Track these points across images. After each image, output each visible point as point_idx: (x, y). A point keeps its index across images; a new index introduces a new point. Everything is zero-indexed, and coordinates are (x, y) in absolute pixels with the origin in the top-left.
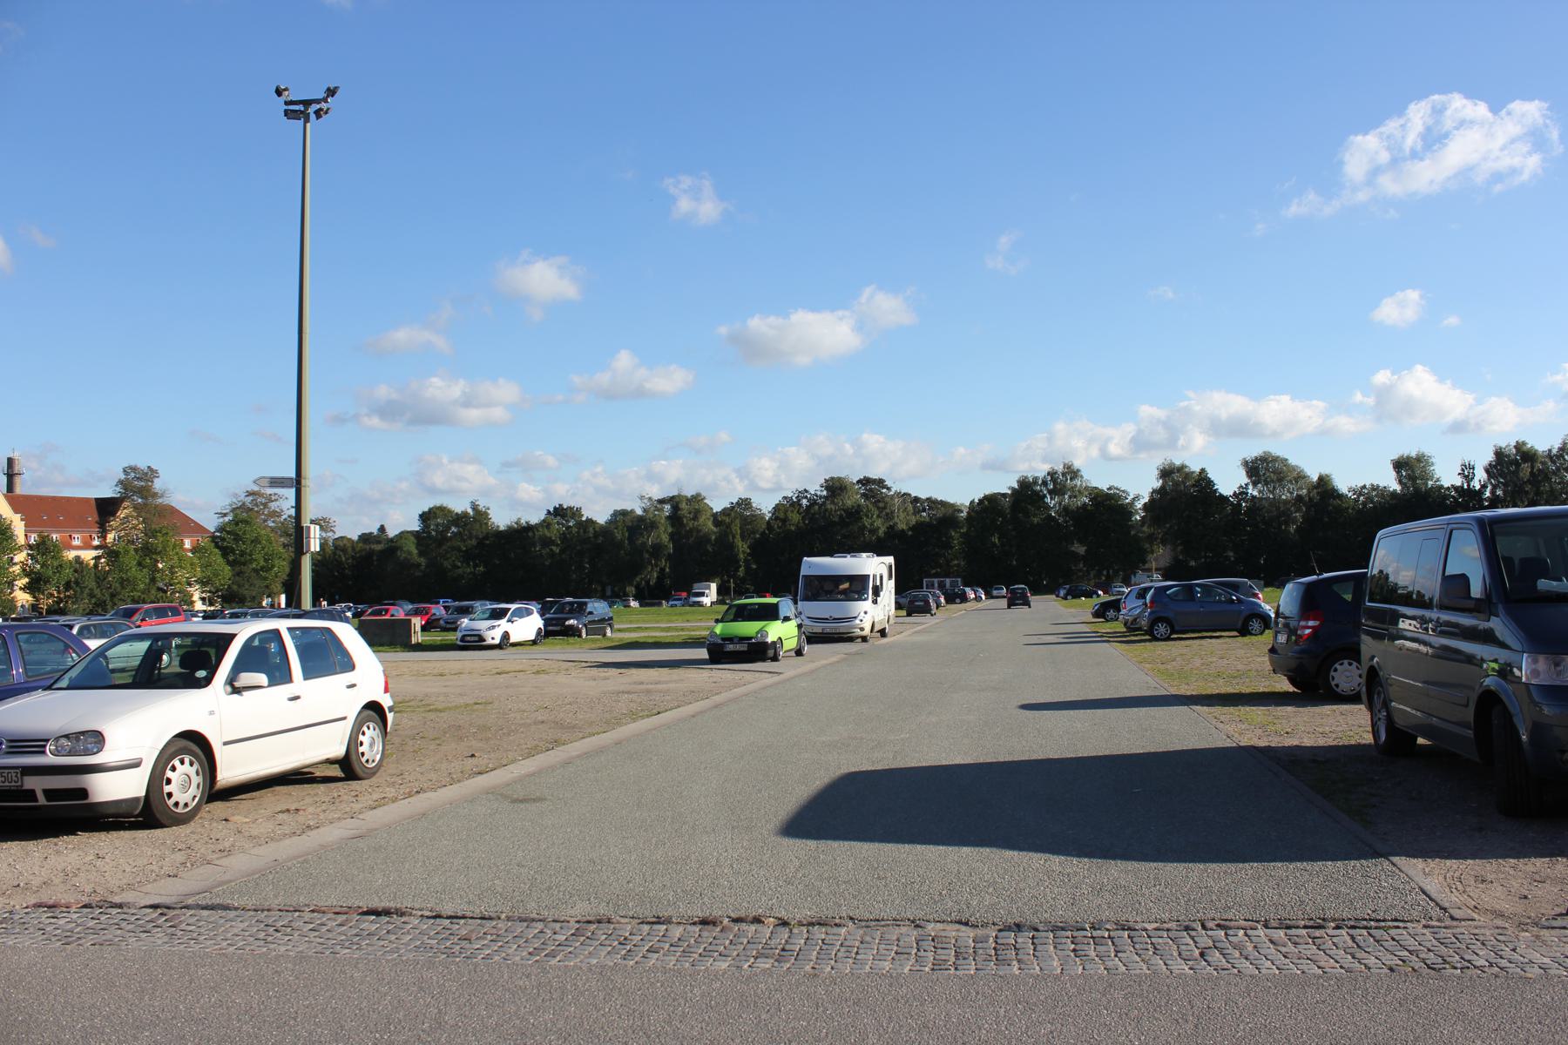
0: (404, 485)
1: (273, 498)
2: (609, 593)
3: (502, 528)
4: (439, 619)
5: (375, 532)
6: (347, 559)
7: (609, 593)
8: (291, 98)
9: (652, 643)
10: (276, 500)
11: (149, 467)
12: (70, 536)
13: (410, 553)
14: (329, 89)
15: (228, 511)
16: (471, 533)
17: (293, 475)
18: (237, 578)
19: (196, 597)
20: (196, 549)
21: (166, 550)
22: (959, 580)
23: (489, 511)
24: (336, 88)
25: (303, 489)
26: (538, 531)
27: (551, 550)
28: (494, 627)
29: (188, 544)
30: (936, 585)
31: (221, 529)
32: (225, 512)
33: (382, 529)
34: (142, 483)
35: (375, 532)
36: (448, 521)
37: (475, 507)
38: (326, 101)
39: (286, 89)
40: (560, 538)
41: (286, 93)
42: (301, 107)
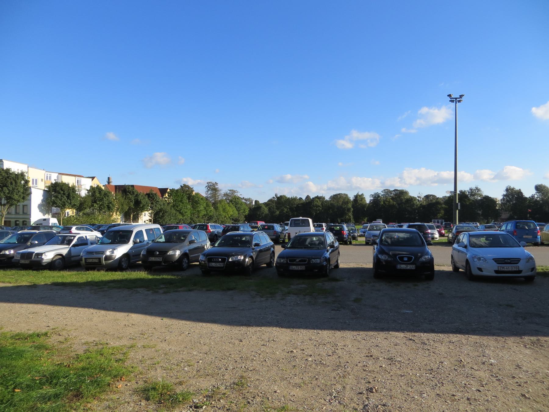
22: (443, 220)
30: (436, 222)
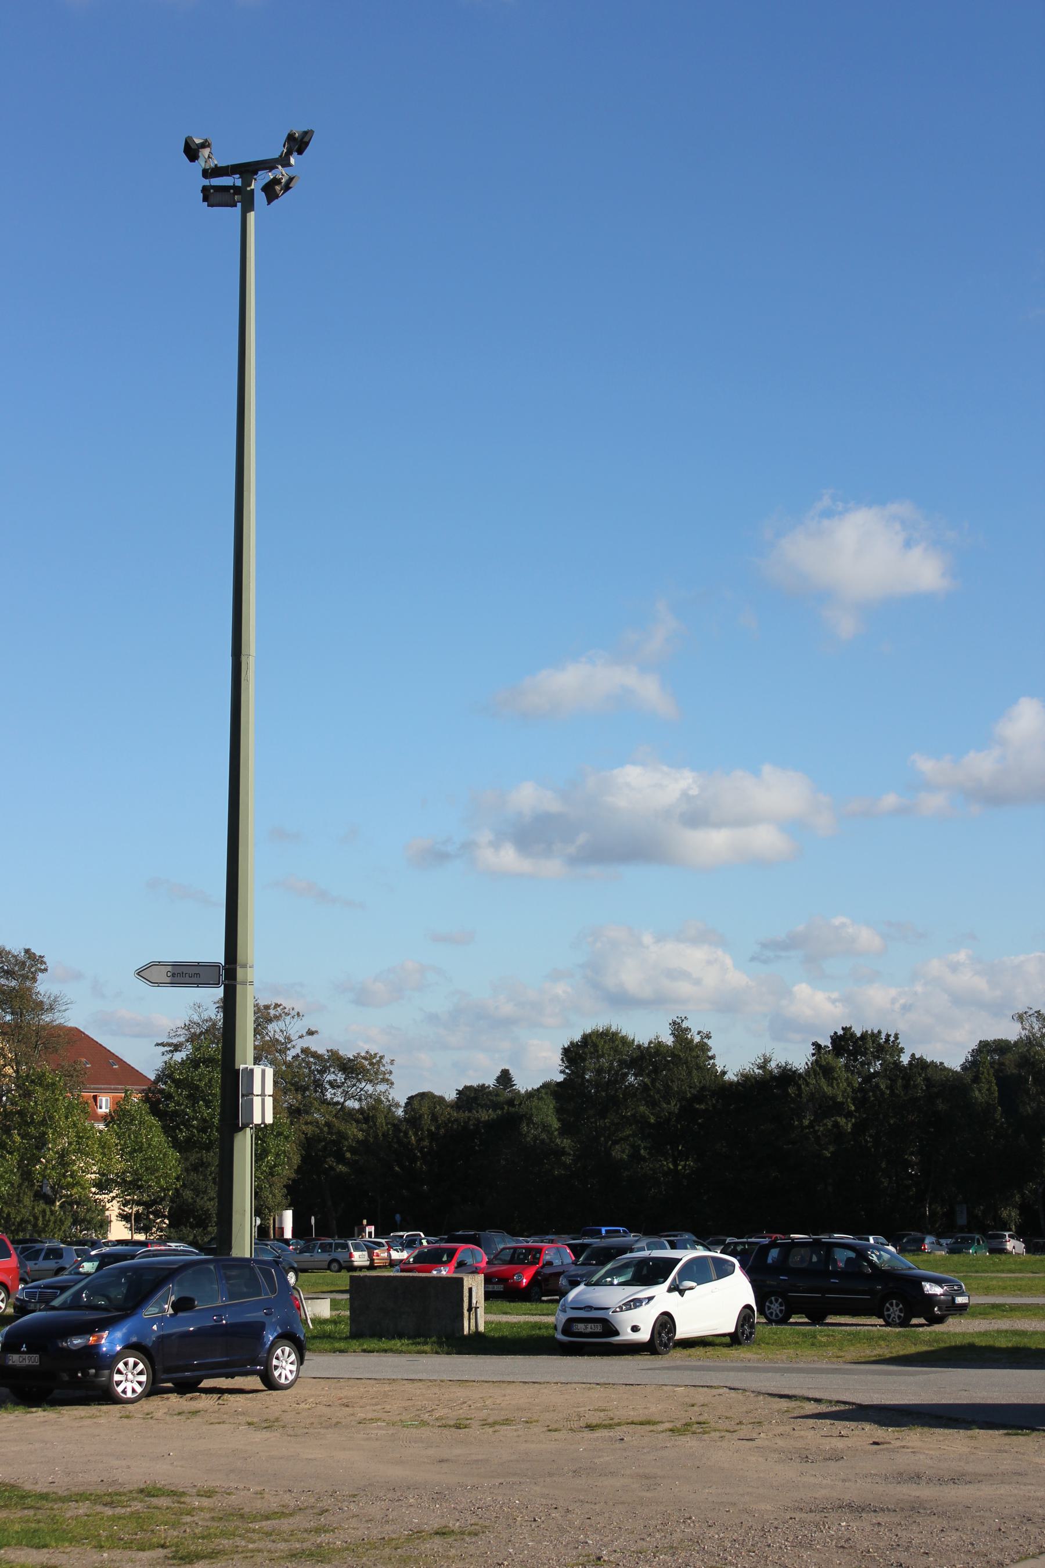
0: (561, 989)
1: (272, 1012)
2: (962, 1220)
3: (731, 1076)
4: (558, 1275)
5: (490, 1081)
6: (420, 1140)
7: (962, 1220)
8: (214, 162)
9: (1007, 1350)
10: (277, 1018)
11: (27, 951)
12: (95, 1098)
13: (546, 1128)
14: (291, 138)
15: (182, 1039)
16: (667, 1087)
17: (219, 957)
18: (193, 1176)
19: (113, 1210)
20: (118, 1117)
21: (51, 1118)
23: (709, 1042)
24: (306, 133)
25: (239, 987)
26: (807, 1084)
27: (836, 1125)
28: (636, 1303)
29: (105, 1105)
31: (167, 1074)
32: (175, 1041)
33: (505, 1078)
34: (13, 983)
35: (490, 1081)
36: (622, 1062)
37: (679, 1031)
38: (286, 164)
39: (205, 145)
40: (854, 1099)
41: (206, 152)
42: (236, 180)
